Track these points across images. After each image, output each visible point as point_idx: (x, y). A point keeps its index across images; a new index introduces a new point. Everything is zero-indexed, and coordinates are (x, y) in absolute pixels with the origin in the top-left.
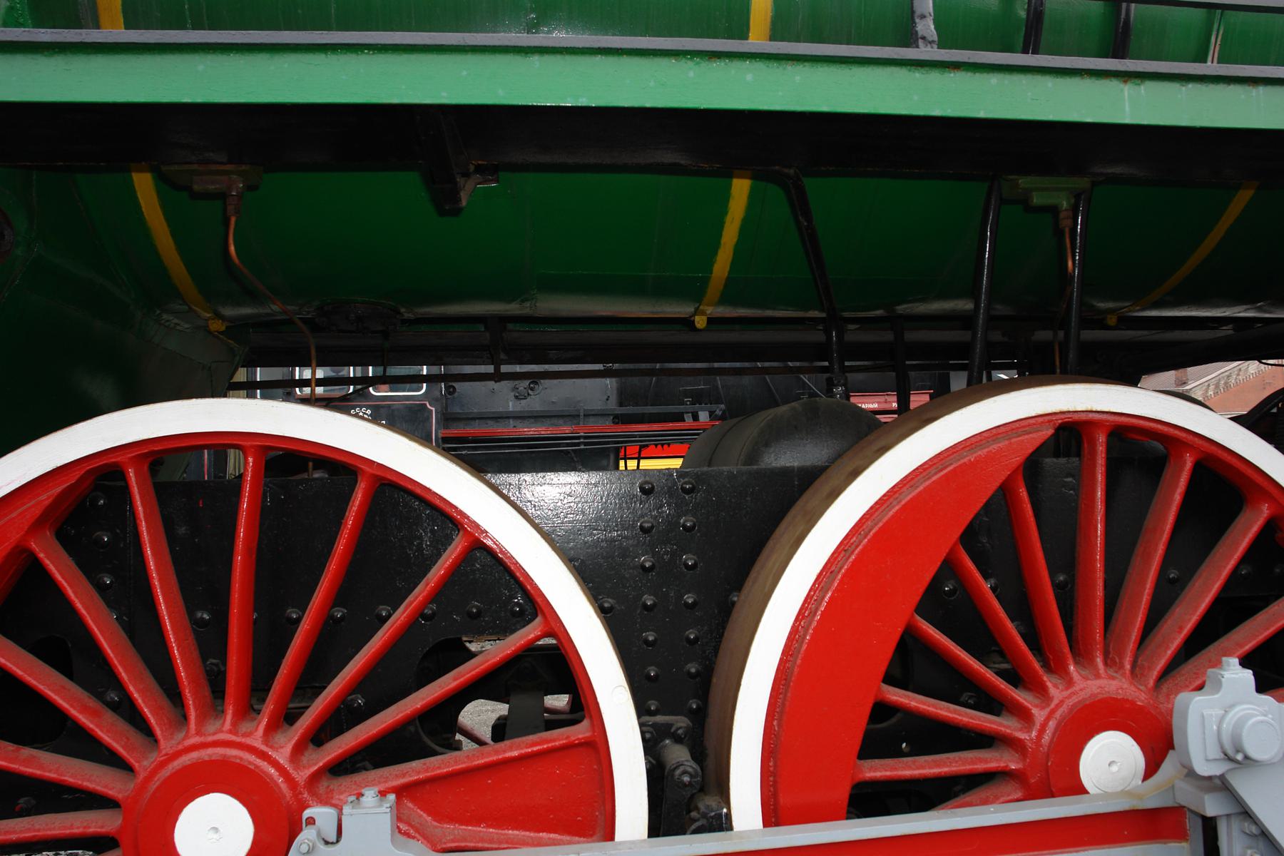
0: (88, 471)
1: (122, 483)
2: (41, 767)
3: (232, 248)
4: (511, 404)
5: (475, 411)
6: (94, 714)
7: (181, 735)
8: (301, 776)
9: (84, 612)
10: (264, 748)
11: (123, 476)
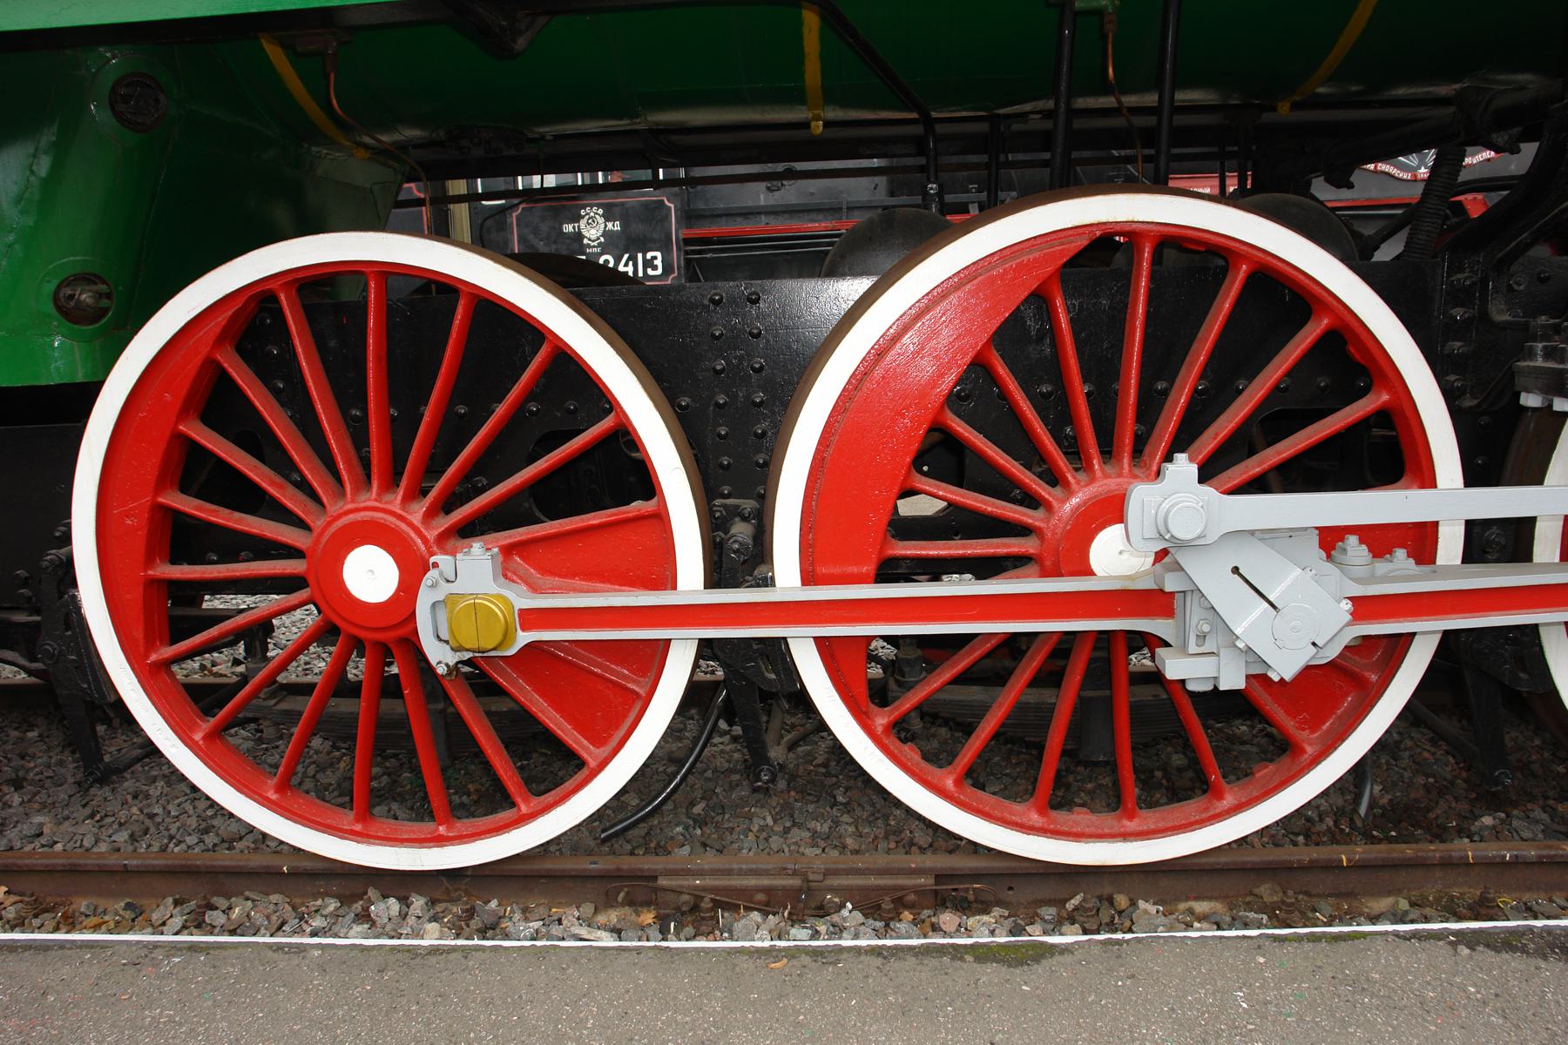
0: (251, 297)
1: (277, 306)
2: (248, 525)
3: (334, 101)
4: (762, 197)
5: (722, 206)
6: (280, 487)
7: (340, 504)
8: (431, 535)
9: (261, 409)
10: (399, 512)
11: (276, 300)
